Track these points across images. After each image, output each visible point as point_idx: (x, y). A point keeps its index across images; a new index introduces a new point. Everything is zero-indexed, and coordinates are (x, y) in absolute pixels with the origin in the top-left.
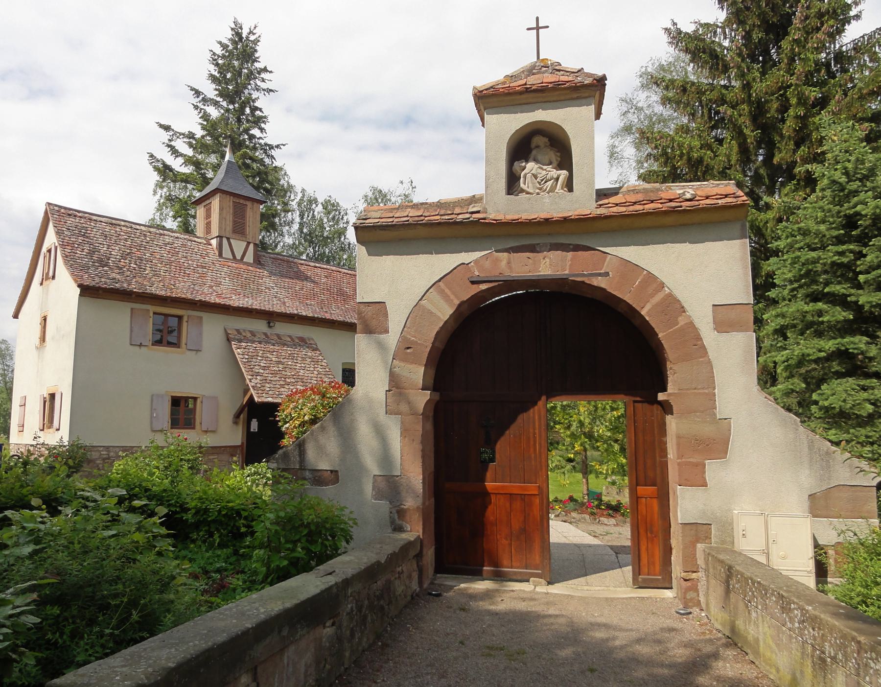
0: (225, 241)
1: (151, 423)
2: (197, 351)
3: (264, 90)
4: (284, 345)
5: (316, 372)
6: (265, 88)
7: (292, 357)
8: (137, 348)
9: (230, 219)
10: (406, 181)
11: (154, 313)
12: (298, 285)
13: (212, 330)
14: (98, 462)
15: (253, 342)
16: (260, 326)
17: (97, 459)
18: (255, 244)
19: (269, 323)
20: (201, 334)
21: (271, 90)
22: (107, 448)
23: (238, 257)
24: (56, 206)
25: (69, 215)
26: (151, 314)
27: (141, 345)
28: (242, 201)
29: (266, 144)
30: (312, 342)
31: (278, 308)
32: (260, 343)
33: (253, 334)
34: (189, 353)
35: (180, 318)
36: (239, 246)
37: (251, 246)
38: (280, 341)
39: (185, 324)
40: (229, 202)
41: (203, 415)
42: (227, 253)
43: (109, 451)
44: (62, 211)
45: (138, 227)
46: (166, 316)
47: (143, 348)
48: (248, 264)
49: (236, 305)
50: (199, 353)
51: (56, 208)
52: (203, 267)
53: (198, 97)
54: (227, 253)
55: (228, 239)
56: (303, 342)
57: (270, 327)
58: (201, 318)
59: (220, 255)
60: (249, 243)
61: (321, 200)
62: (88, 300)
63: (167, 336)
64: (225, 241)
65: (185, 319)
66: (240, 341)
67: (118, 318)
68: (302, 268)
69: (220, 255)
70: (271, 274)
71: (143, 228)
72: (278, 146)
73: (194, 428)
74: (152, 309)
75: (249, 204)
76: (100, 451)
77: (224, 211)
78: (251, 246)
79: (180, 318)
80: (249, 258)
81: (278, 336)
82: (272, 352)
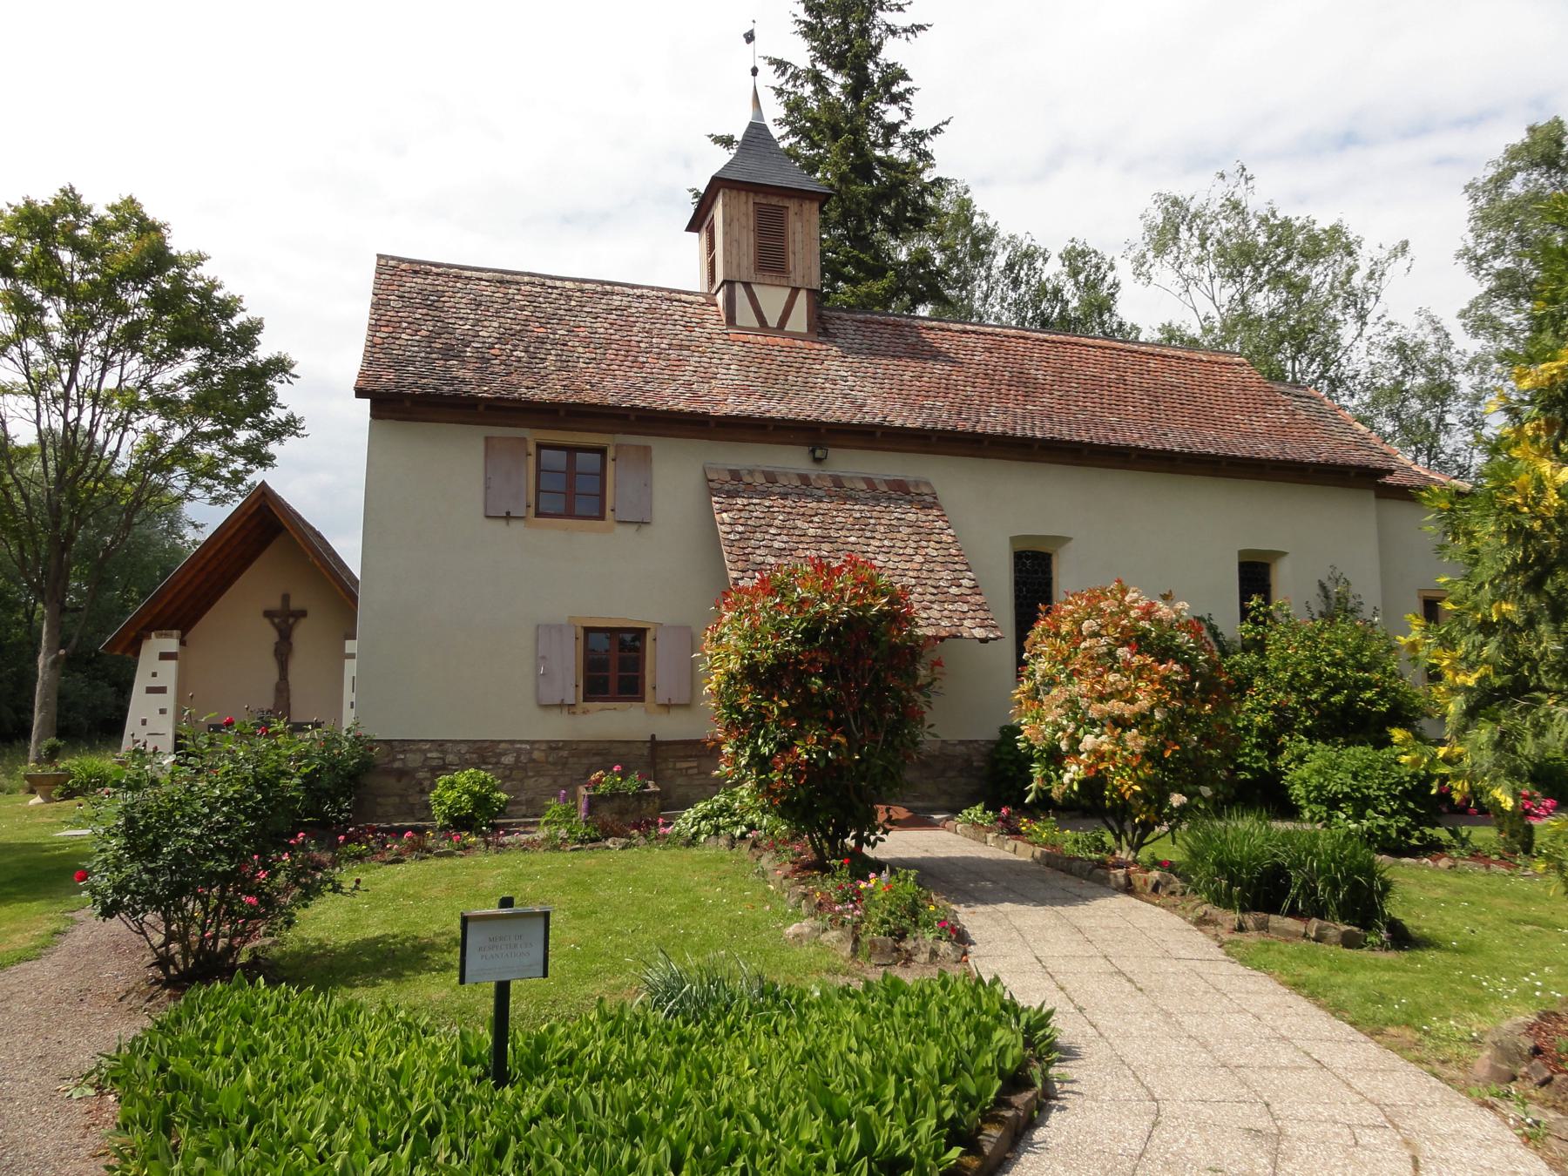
0: (740, 291)
1: (537, 687)
2: (642, 523)
3: (905, 30)
4: (846, 499)
5: (919, 559)
6: (908, 25)
7: (862, 525)
8: (502, 523)
9: (748, 241)
10: (1231, 168)
11: (540, 447)
12: (909, 370)
13: (675, 473)
14: (421, 775)
15: (765, 495)
16: (792, 460)
17: (416, 770)
18: (810, 292)
19: (813, 451)
20: (648, 485)
21: (920, 27)
22: (440, 744)
23: (773, 322)
24: (393, 258)
25: (416, 272)
26: (532, 449)
27: (508, 517)
28: (774, 201)
29: (914, 134)
30: (925, 490)
31: (837, 412)
32: (784, 496)
33: (771, 478)
34: (620, 529)
35: (602, 451)
36: (772, 300)
37: (802, 298)
38: (840, 491)
39: (610, 466)
40: (746, 206)
41: (659, 666)
42: (745, 315)
43: (444, 752)
44: (403, 266)
45: (558, 283)
46: (572, 450)
47: (514, 524)
48: (794, 336)
49: (723, 410)
50: (645, 529)
51: (392, 263)
52: (681, 347)
53: (783, 74)
54: (745, 315)
55: (747, 285)
56: (901, 491)
57: (817, 461)
58: (647, 449)
59: (731, 320)
60: (795, 291)
61: (1056, 248)
62: (386, 425)
63: (574, 496)
64: (740, 291)
65: (610, 454)
66: (732, 495)
67: (458, 458)
68: (929, 336)
69: (731, 320)
70: (848, 351)
71: (569, 285)
72: (936, 130)
73: (642, 699)
74: (532, 436)
75: (793, 206)
76: (424, 752)
77: (736, 225)
78: (802, 298)
79: (602, 451)
80: (799, 320)
81: (838, 482)
82: (809, 518)
